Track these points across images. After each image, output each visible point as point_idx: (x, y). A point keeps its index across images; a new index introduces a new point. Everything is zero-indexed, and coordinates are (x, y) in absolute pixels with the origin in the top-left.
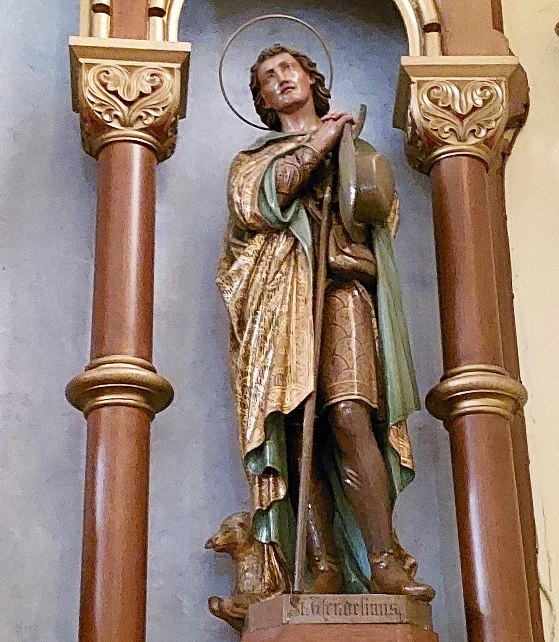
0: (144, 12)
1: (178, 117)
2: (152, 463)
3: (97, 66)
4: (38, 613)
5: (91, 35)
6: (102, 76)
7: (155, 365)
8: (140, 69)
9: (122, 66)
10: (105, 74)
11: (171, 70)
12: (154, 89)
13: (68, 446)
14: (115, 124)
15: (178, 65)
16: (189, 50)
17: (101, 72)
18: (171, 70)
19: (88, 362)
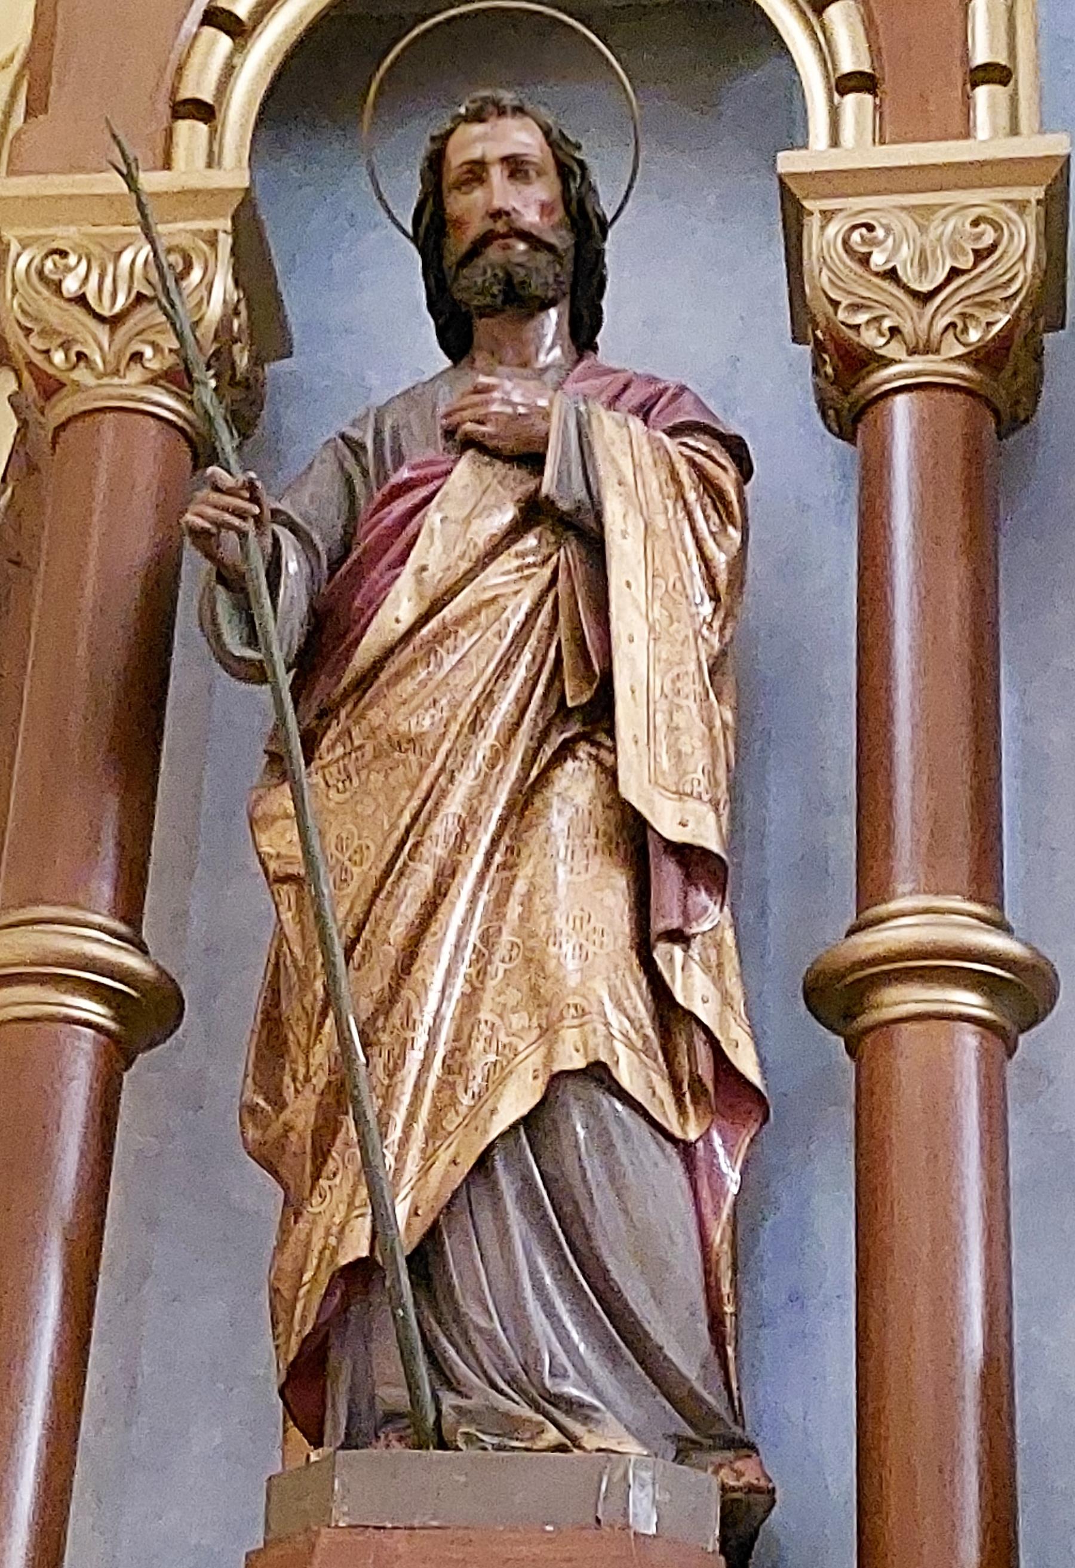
0: (958, 75)
1: (1042, 322)
2: (612, 1252)
3: (841, 215)
4: (695, 1509)
5: (167, 165)
6: (856, 237)
7: (1008, 916)
8: (944, 212)
9: (903, 208)
10: (864, 230)
11: (1021, 206)
12: (980, 255)
13: (45, 1180)
14: (894, 350)
15: (1037, 193)
16: (1062, 151)
17: (855, 227)
18: (1021, 206)
19: (850, 920)
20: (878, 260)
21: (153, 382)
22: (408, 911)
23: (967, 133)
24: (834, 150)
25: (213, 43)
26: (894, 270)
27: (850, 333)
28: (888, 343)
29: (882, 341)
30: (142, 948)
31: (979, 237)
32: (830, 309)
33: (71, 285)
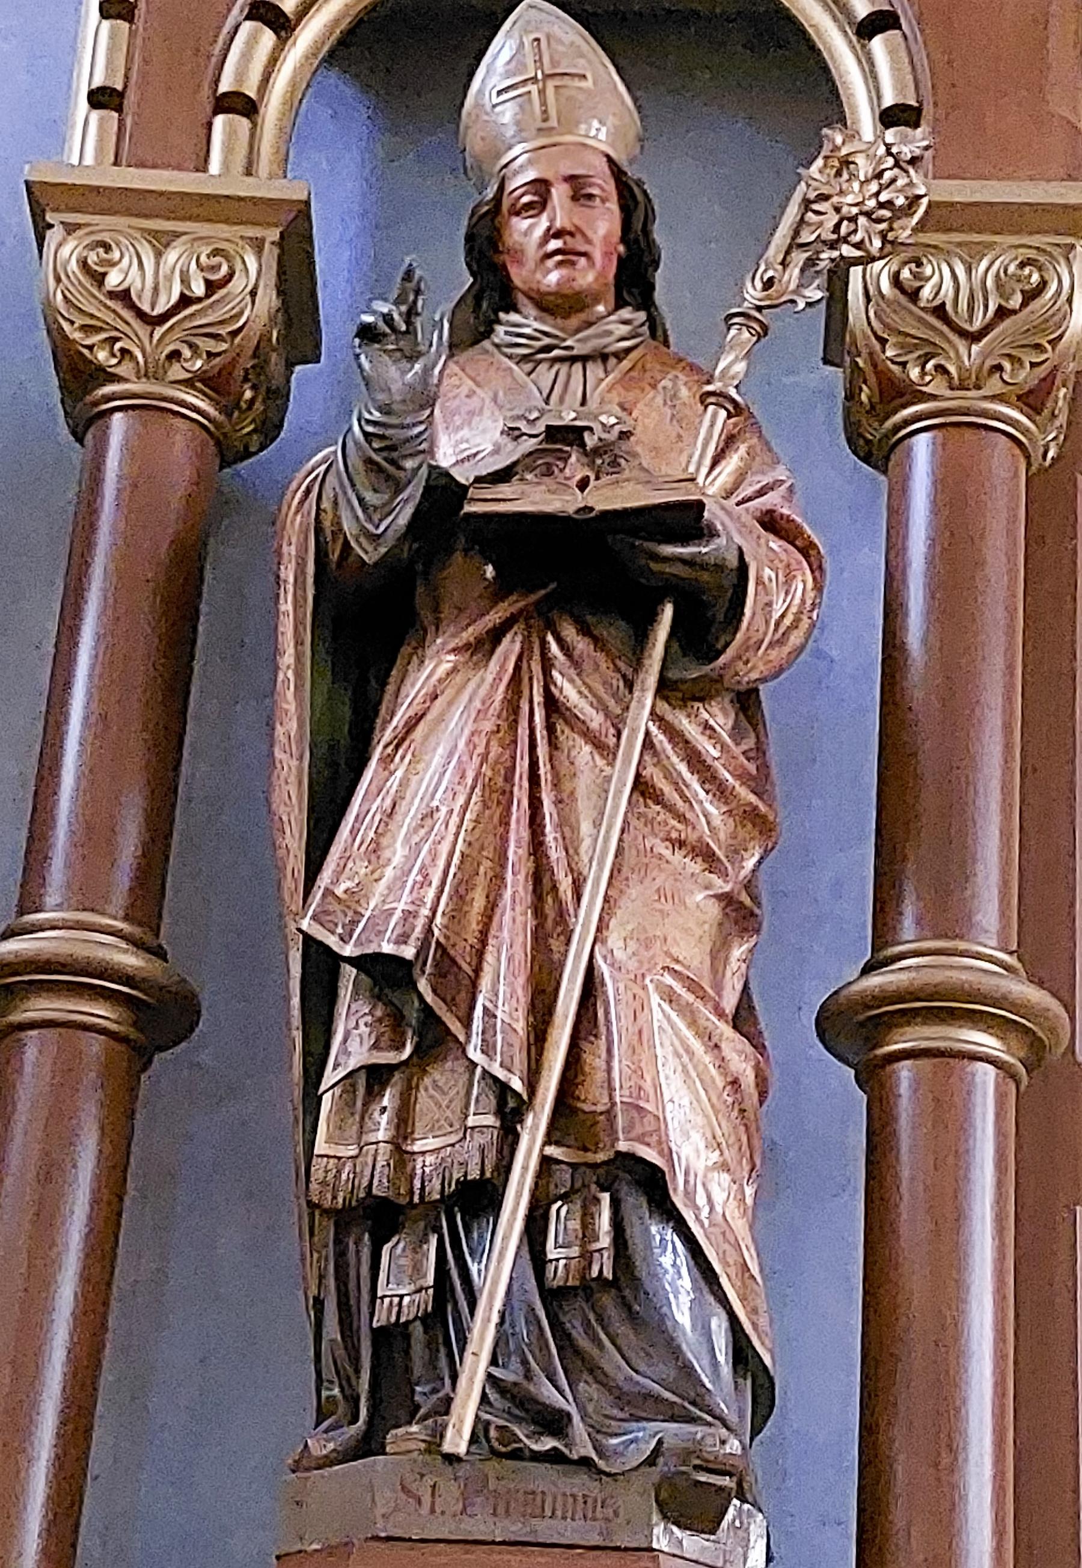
12: (211, 287)
14: (124, 370)
20: (113, 279)
21: (188, 383)
22: (474, 925)
23: (202, 166)
24: (246, 178)
25: (253, 41)
26: (127, 291)
27: (86, 352)
28: (119, 362)
29: (114, 361)
30: (159, 953)
31: (216, 268)
32: (877, 347)
33: (113, 279)
